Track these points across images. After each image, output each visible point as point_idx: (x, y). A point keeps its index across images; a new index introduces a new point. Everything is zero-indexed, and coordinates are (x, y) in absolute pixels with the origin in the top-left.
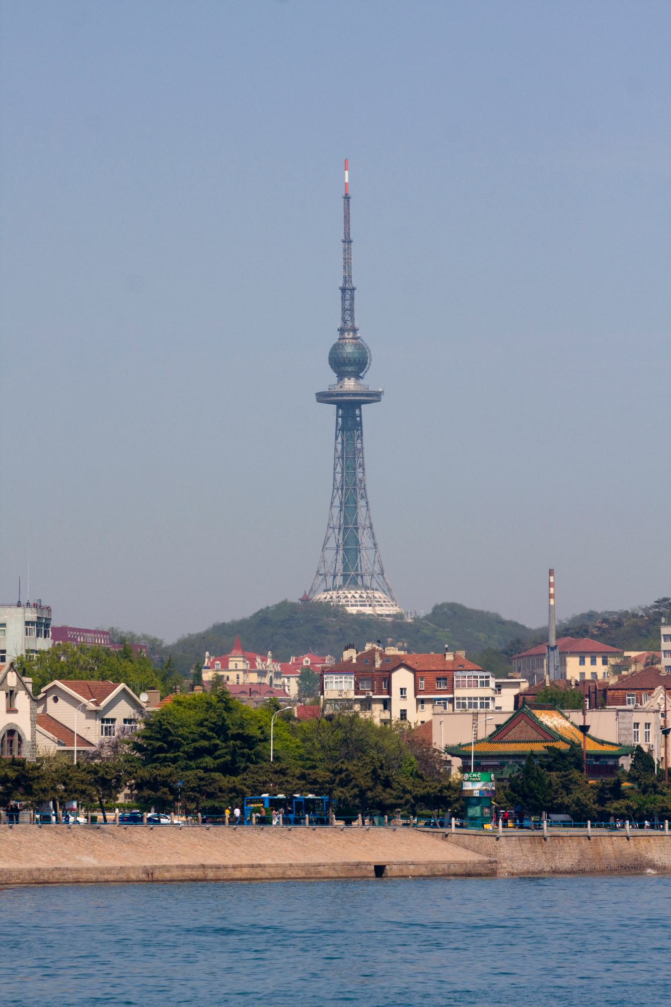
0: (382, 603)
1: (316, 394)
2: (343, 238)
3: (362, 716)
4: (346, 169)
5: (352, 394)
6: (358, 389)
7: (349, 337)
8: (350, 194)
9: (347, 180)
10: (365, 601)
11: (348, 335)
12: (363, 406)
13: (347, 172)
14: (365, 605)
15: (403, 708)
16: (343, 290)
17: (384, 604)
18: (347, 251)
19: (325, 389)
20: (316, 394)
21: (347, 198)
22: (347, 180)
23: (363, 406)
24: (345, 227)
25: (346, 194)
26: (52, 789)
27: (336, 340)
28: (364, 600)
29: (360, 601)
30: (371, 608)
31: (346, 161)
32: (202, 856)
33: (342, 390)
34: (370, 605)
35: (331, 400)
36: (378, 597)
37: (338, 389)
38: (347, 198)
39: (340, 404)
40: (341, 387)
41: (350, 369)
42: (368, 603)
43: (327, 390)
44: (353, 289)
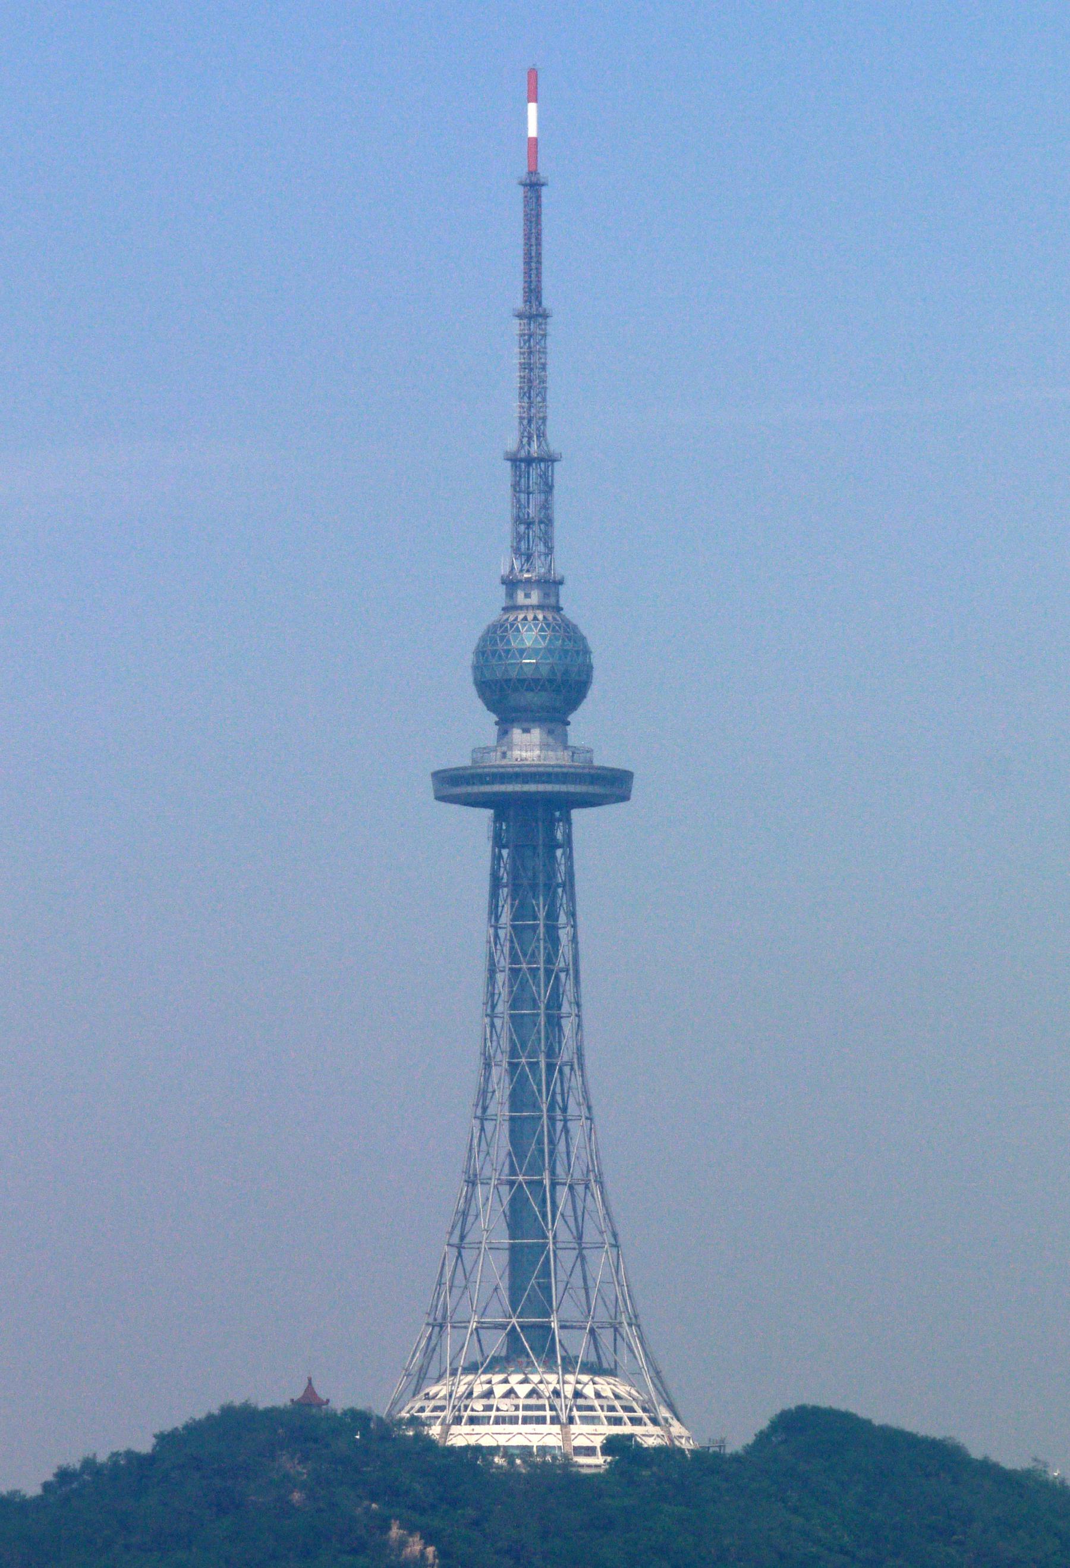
0: (621, 1413)
1: (435, 775)
2: (519, 304)
3: (349, 1414)
4: (534, 143)
5: (541, 774)
6: (557, 758)
7: (528, 602)
8: (545, 171)
9: (532, 108)
10: (542, 1408)
11: (527, 596)
12: (576, 814)
13: (532, 132)
14: (541, 1420)
15: (637, 787)
16: (520, 462)
17: (625, 1415)
18: (533, 292)
19: (460, 759)
20: (435, 775)
21: (533, 186)
22: (532, 108)
23: (576, 814)
24: (528, 237)
25: (533, 172)
26: (131, 1079)
27: (493, 613)
28: (540, 1402)
29: (526, 1408)
30: (556, 1428)
31: (533, 75)
32: (65, 1134)
33: (504, 762)
34: (555, 1420)
35: (477, 794)
36: (592, 1394)
37: (494, 760)
38: (533, 186)
39: (500, 805)
40: (504, 755)
41: (532, 698)
42: (548, 1414)
43: (468, 763)
44: (549, 460)
